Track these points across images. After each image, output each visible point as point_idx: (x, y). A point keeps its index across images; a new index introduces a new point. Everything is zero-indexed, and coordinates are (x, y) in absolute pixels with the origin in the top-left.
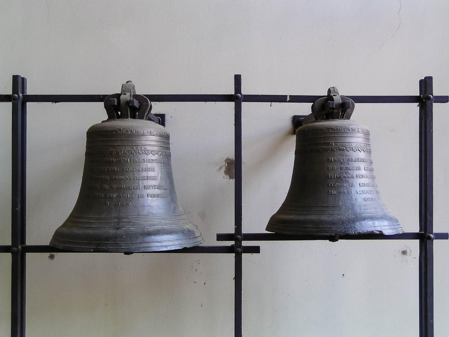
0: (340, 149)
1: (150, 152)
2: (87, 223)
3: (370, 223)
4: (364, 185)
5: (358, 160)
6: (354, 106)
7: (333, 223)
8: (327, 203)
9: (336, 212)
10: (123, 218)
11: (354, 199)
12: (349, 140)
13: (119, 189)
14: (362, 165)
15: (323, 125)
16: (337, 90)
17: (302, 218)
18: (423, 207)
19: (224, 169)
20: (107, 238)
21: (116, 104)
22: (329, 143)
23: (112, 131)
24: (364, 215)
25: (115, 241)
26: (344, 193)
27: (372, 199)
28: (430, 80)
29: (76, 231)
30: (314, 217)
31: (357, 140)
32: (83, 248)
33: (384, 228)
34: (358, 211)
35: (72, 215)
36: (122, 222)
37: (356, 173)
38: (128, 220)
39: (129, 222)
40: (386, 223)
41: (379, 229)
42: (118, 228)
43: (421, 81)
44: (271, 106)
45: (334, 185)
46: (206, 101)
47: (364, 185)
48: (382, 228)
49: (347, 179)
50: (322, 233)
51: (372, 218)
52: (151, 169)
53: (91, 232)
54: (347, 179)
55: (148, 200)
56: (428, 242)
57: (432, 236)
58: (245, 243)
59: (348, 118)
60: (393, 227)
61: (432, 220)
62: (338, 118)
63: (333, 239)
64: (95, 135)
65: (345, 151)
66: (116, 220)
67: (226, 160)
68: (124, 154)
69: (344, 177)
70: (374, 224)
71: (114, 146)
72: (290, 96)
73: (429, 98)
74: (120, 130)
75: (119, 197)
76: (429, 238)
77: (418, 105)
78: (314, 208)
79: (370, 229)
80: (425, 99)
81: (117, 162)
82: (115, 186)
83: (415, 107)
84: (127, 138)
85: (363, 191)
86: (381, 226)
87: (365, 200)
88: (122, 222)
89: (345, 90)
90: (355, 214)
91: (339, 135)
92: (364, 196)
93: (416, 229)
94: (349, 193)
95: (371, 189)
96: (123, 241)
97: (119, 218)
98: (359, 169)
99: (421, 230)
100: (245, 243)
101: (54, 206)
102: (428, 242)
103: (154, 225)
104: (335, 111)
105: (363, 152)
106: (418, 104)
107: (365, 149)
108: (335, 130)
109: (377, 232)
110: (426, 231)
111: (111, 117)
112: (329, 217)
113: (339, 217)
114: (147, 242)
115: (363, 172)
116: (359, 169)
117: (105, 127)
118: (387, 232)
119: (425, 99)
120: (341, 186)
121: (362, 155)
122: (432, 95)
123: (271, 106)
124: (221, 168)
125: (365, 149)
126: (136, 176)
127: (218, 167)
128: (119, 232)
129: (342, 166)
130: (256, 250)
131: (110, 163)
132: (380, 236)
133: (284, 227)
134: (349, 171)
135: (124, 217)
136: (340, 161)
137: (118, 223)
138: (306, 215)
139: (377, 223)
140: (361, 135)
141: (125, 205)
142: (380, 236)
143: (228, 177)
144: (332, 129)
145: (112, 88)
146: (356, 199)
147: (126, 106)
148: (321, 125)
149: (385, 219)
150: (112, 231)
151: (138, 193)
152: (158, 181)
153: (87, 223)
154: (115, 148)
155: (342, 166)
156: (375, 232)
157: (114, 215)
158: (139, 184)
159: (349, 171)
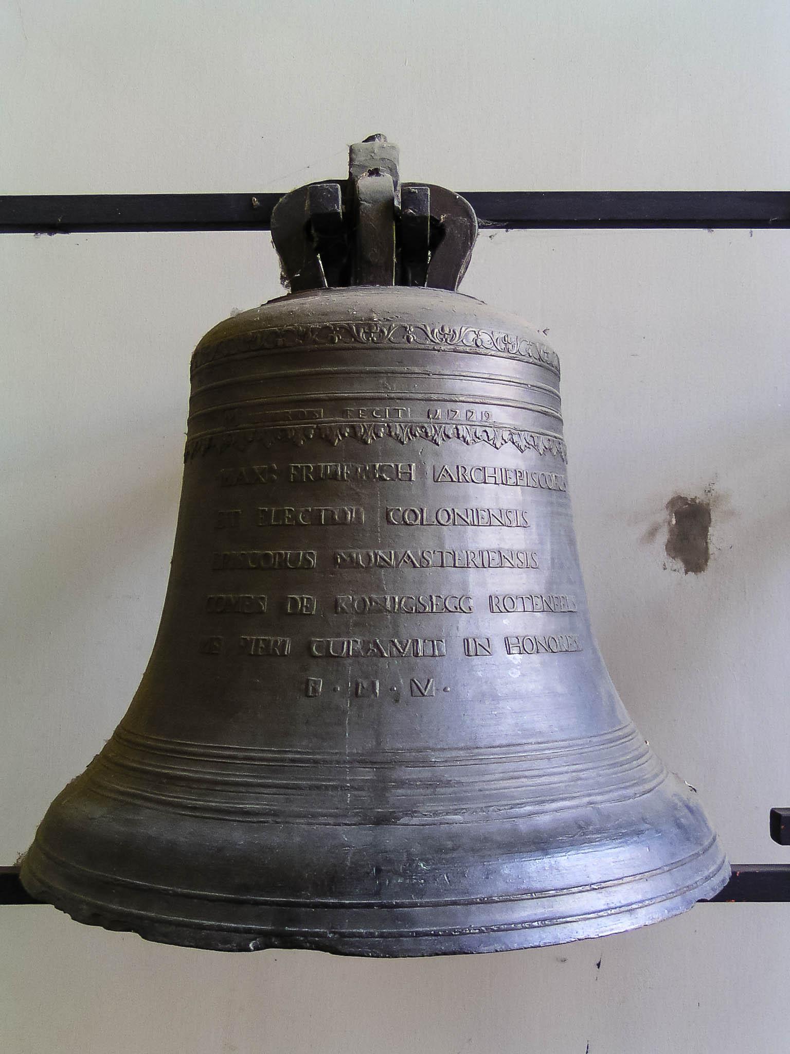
1: (506, 436)
2: (212, 786)
10: (401, 763)
13: (371, 614)
19: (663, 537)
20: (333, 879)
21: (340, 208)
23: (326, 332)
25: (377, 894)
29: (156, 827)
31: (489, 386)
32: (202, 927)
35: (124, 737)
36: (402, 784)
38: (425, 773)
39: (433, 784)
42: (382, 820)
46: (710, 224)
52: (512, 516)
53: (238, 836)
55: (510, 665)
59: (448, 280)
64: (232, 364)
66: (367, 774)
68: (391, 442)
71: (338, 405)
74: (368, 324)
75: (373, 651)
81: (354, 477)
82: (347, 599)
84: (401, 363)
88: (402, 784)
89: (440, 159)
96: (421, 893)
97: (381, 763)
103: (543, 797)
111: (299, 278)
114: (540, 894)
117: (279, 317)
124: (652, 533)
126: (448, 547)
127: (644, 528)
128: (392, 837)
131: (323, 486)
135: (408, 756)
137: (380, 788)
141: (405, 692)
143: (679, 565)
145: (280, 173)
147: (366, 235)
150: (352, 837)
151: (462, 634)
152: (547, 573)
153: (212, 786)
154: (344, 413)
157: (354, 743)
158: (465, 584)
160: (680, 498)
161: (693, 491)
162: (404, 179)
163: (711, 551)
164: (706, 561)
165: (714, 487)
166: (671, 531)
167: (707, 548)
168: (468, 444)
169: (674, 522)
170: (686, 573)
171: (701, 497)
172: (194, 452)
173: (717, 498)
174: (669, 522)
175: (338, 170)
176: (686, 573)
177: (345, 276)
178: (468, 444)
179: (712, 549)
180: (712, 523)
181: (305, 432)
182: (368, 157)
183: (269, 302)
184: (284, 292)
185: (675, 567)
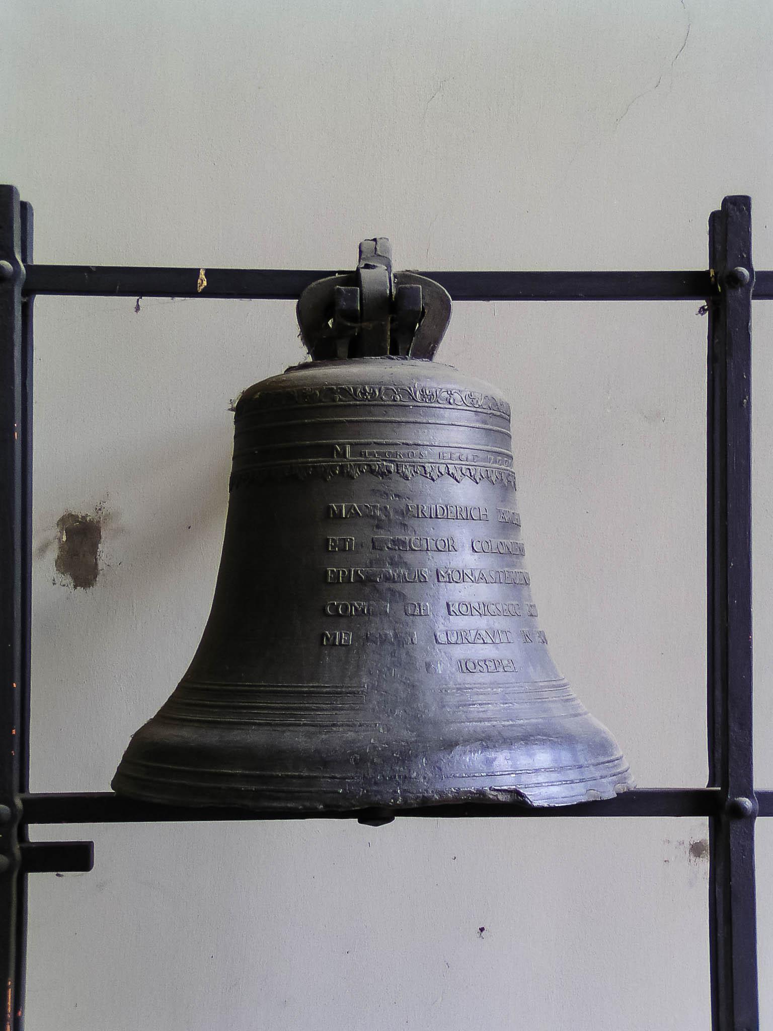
0: (372, 471)
3: (473, 759)
4: (469, 609)
5: (448, 513)
6: (448, 309)
7: (322, 761)
8: (312, 680)
9: (342, 717)
11: (420, 664)
12: (409, 435)
14: (462, 533)
15: (314, 377)
16: (387, 250)
17: (212, 737)
18: (718, 693)
22: (332, 447)
24: (453, 727)
26: (384, 640)
27: (497, 663)
28: (741, 211)
29: (187, 735)
30: (255, 737)
31: (450, 436)
33: (534, 779)
34: (433, 711)
37: (441, 560)
40: (543, 757)
41: (508, 782)
43: (715, 218)
44: (138, 308)
45: (345, 608)
47: (469, 609)
48: (524, 779)
49: (398, 587)
50: (278, 799)
51: (488, 741)
54: (398, 587)
56: (736, 827)
57: (747, 803)
58: (40, 833)
59: (427, 352)
60: (572, 775)
61: (750, 744)
62: (379, 352)
63: (374, 814)
65: (396, 477)
67: (63, 521)
69: (388, 579)
70: (489, 762)
72: (209, 272)
73: (735, 280)
76: (738, 812)
77: (702, 310)
78: (293, 698)
79: (472, 785)
80: (721, 288)
83: (689, 319)
85: (459, 633)
86: (516, 772)
87: (465, 666)
89: (418, 251)
90: (416, 720)
91: (370, 413)
92: (460, 652)
93: (696, 776)
94: (401, 641)
95: (500, 623)
98: (449, 547)
99: (712, 783)
100: (40, 833)
101: (109, 673)
102: (736, 827)
104: (368, 325)
105: (467, 481)
106: (703, 303)
107: (478, 472)
108: (354, 396)
109: (502, 797)
110: (725, 785)
112: (309, 735)
113: (350, 735)
115: (465, 559)
116: (449, 547)
118: (537, 797)
119: (721, 288)
120: (374, 615)
121: (465, 493)
122: (749, 267)
123: (138, 308)
125: (478, 472)
129: (382, 535)
130: (77, 858)
132: (516, 806)
133: (180, 774)
134: (409, 557)
136: (374, 517)
138: (231, 725)
139: (502, 759)
140: (465, 417)
142: (516, 806)
143: (68, 580)
144: (344, 392)
146: (428, 666)
147: (369, 315)
148: (306, 378)
149: (543, 742)
155: (382, 535)
156: (491, 795)
159: (409, 557)
160: (70, 515)
161: (83, 508)
162: (397, 268)
163: (100, 567)
164: (95, 577)
165: (104, 505)
166: (61, 548)
167: (96, 564)
168: (433, 480)
169: (64, 539)
170: (75, 587)
171: (91, 515)
172: (236, 481)
173: (108, 515)
174: (60, 539)
175: (350, 264)
176: (75, 587)
177: (358, 350)
178: (433, 480)
179: (101, 565)
180: (102, 540)
181: (332, 468)
182: (372, 252)
183: (290, 369)
184: (310, 359)
185: (64, 582)
